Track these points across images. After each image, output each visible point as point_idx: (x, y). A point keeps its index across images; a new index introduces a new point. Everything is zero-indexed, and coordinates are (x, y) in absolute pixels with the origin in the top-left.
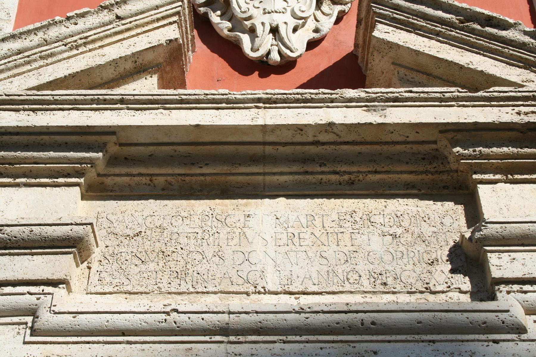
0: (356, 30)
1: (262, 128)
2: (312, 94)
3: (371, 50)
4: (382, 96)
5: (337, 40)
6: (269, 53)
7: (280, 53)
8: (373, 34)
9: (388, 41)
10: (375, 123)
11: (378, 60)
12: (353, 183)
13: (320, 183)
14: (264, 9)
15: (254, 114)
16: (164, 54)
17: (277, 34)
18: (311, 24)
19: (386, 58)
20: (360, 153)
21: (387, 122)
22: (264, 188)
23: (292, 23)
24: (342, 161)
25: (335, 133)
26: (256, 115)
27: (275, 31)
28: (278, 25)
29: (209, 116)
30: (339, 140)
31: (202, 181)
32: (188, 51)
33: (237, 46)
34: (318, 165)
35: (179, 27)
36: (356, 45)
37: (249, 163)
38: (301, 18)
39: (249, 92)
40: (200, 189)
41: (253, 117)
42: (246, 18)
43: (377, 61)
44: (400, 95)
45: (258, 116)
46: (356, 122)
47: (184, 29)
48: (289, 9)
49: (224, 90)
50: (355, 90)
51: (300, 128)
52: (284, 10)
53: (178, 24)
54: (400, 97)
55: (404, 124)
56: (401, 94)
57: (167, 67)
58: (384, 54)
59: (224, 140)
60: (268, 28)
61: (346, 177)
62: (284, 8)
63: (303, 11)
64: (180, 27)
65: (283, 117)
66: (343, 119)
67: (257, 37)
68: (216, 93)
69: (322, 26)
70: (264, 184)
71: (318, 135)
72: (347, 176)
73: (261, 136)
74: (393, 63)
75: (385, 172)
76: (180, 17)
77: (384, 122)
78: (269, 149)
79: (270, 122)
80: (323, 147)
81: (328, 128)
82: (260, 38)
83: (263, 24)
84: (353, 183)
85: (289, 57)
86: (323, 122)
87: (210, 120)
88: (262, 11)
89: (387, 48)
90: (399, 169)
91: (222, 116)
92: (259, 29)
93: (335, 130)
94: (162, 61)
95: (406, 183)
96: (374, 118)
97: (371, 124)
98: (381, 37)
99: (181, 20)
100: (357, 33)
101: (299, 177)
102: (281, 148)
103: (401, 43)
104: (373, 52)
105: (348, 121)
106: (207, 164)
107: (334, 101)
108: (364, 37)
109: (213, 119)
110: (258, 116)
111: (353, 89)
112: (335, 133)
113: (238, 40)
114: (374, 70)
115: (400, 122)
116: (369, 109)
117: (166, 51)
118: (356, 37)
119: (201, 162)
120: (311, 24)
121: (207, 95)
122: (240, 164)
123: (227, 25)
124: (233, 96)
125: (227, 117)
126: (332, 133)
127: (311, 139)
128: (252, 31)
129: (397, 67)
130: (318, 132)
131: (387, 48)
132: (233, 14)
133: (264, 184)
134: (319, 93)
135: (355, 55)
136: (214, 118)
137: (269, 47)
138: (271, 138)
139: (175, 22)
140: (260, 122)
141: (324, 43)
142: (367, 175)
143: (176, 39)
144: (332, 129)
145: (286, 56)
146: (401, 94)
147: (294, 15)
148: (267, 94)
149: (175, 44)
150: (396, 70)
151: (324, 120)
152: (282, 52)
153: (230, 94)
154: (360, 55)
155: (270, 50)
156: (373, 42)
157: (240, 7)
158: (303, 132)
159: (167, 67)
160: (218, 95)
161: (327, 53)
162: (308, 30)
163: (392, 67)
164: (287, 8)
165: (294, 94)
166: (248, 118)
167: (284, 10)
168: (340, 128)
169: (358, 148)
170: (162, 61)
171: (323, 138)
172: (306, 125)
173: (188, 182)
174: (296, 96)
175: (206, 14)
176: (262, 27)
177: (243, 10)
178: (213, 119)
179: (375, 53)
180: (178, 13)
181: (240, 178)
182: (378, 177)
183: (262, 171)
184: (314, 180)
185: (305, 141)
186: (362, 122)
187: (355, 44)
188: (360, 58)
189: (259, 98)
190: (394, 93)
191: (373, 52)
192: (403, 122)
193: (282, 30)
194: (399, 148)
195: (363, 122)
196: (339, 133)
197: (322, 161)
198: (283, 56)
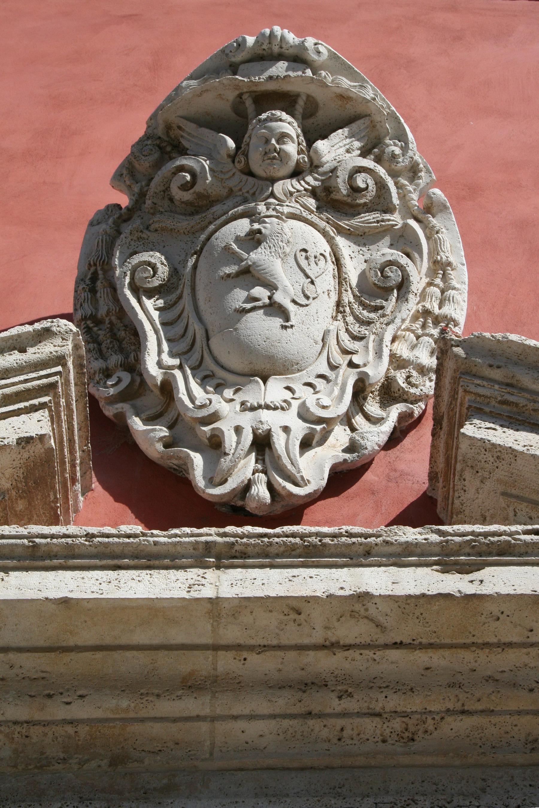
0: (433, 441)
1: (209, 606)
2: (326, 535)
3: (459, 467)
4: (475, 541)
5: (395, 470)
6: (247, 487)
7: (270, 486)
8: (462, 430)
9: (493, 444)
10: (458, 595)
11: (473, 491)
12: (413, 740)
13: (339, 740)
14: (243, 403)
15: (195, 577)
16: (10, 471)
17: (267, 450)
18: (340, 436)
19: (489, 485)
20: (427, 669)
21: (484, 592)
22: (211, 754)
23: (300, 429)
24: (387, 687)
25: (372, 620)
26: (199, 578)
27: (262, 444)
28: (270, 430)
29: (93, 581)
30: (382, 639)
31: (69, 737)
32: (74, 481)
33: (177, 478)
34: (333, 695)
35: (51, 417)
36: (433, 476)
37: (180, 693)
38: (320, 421)
39: (187, 530)
40: (62, 755)
41: (192, 582)
42: (203, 418)
43: (471, 493)
44: (515, 539)
45: (203, 581)
46: (418, 593)
47: (64, 426)
48: (295, 404)
49: (130, 527)
50: (419, 529)
51: (294, 608)
52: (284, 405)
53: (50, 411)
54: (513, 542)
55: (522, 596)
56: (517, 537)
57: (20, 502)
58: (486, 474)
59: (124, 640)
60: (248, 438)
61: (397, 724)
62: (285, 401)
63: (324, 407)
64: (55, 419)
65: (258, 582)
66: (390, 587)
67: (226, 454)
68: (113, 531)
69: (363, 438)
70: (213, 744)
71: (336, 624)
72: (398, 720)
73: (209, 627)
74: (504, 494)
75: (482, 711)
76: (56, 396)
77: (479, 592)
78: (226, 662)
79: (227, 592)
80: (347, 653)
81: (358, 607)
82: (230, 457)
83: (238, 430)
84: (413, 740)
85: (291, 494)
86: (347, 593)
87: (95, 589)
88: (238, 407)
89: (492, 460)
90: (513, 706)
91: (122, 581)
92: (230, 440)
93: (372, 611)
94: (8, 485)
95: (530, 738)
96: (455, 584)
97: (448, 596)
98: (479, 436)
99: (57, 404)
100: (434, 446)
101: (291, 723)
102: (254, 659)
103: (520, 448)
104: (462, 470)
105: (401, 591)
106: (81, 696)
107: (373, 551)
108: (447, 451)
109: (101, 587)
110: (203, 581)
111: (414, 527)
112: (372, 620)
113: (185, 464)
114: (467, 512)
115: (512, 592)
116: (446, 568)
117: (16, 463)
118: (432, 457)
119: (68, 690)
120: (340, 436)
121: (93, 536)
122: (158, 696)
123: (162, 434)
124: (151, 539)
125: (133, 584)
126: (366, 621)
127: (318, 637)
128: (215, 446)
129: (513, 500)
130: (335, 618)
131: (492, 460)
132: (179, 415)
133: (213, 744)
134: (341, 535)
135: (431, 498)
136: (104, 586)
137: (249, 475)
138: (231, 634)
139: (42, 406)
140: (208, 592)
141: (369, 476)
142: (442, 718)
143: (41, 438)
144: (367, 610)
145: (283, 493)
146: (517, 537)
147: (304, 415)
148: (225, 535)
149: (38, 449)
150: (511, 508)
151: (347, 589)
152: (276, 486)
153: (144, 535)
154: (439, 497)
155: (250, 480)
156: (464, 446)
157: (192, 399)
158: (302, 617)
159: (20, 502)
160: (118, 536)
161: (373, 493)
162: (334, 446)
163: (502, 502)
164: (292, 401)
165: (287, 536)
166: (180, 585)
167: (284, 405)
168: (383, 607)
169: (422, 658)
170: (8, 485)
171: (350, 631)
172: (307, 600)
173: (35, 739)
174: (291, 539)
175: (121, 417)
176: (234, 438)
177: (198, 403)
178: (101, 587)
179: (467, 475)
180: (53, 386)
181: (157, 729)
182: (468, 722)
183: (206, 711)
184: (325, 733)
185: (306, 641)
186: (430, 593)
187: (430, 474)
188: (440, 499)
189: (207, 543)
190: (500, 535)
191: (462, 470)
192: (519, 592)
193: (279, 441)
194: (513, 657)
195: (434, 591)
196: (382, 619)
197: (345, 687)
198: (279, 494)
